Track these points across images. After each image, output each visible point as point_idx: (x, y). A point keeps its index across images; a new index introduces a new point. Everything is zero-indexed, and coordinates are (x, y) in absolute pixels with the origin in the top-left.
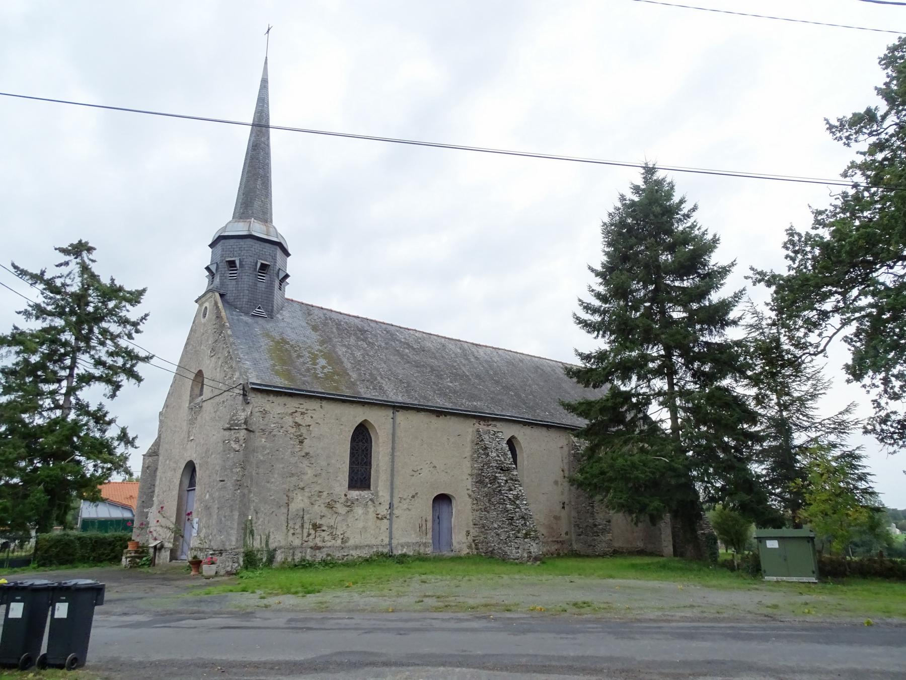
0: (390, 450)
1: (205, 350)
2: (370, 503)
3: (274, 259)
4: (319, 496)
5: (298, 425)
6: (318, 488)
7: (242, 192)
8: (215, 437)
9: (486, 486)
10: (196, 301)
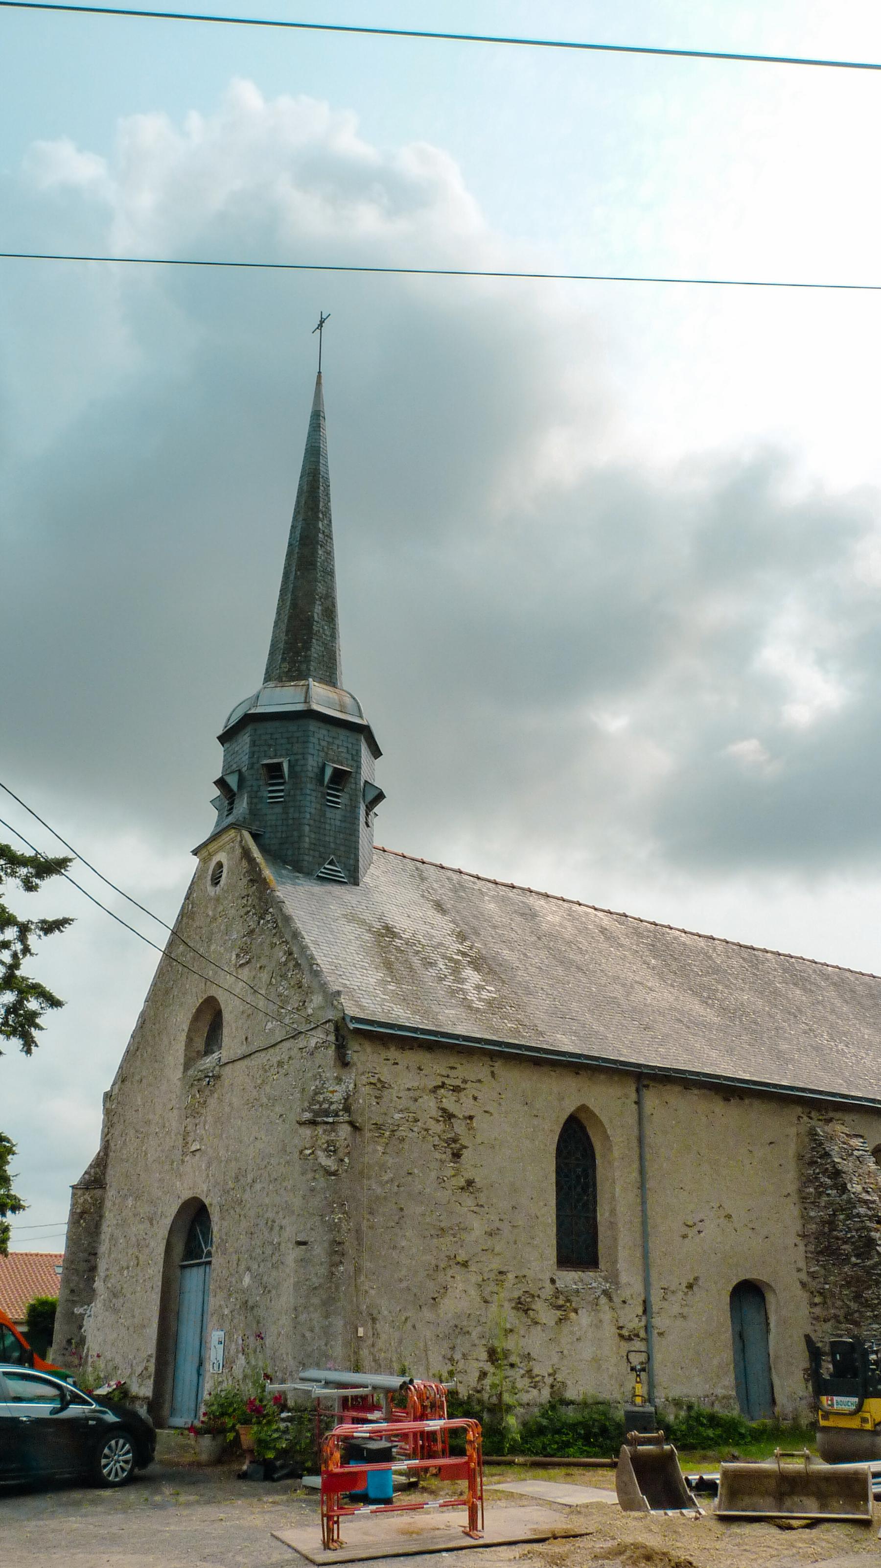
0: (635, 1175)
1: (223, 950)
2: (603, 1300)
3: (356, 758)
4: (500, 1283)
5: (448, 1116)
6: (496, 1264)
7: (284, 627)
8: (259, 1145)
9: (847, 1261)
10: (195, 852)
